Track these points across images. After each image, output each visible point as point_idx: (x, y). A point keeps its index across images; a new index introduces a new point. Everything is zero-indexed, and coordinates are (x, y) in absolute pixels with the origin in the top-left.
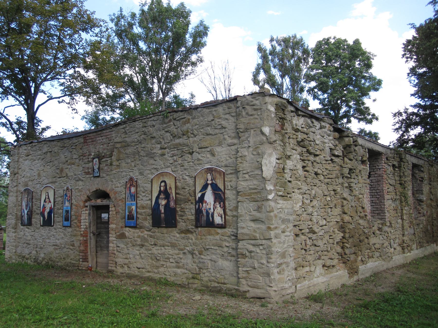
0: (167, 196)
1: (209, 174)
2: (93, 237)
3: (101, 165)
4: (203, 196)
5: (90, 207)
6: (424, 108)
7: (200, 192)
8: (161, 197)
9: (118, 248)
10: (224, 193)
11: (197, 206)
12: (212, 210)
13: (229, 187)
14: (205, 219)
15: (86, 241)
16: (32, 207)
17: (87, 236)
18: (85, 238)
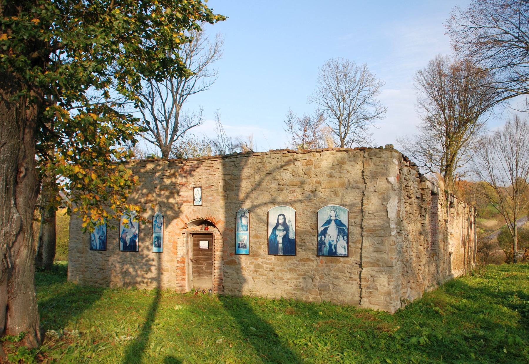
0: (286, 228)
1: (333, 212)
2: (191, 264)
3: (203, 195)
4: (326, 230)
5: (188, 235)
6: (118, 139)
7: (323, 226)
8: (278, 228)
9: (226, 274)
10: (348, 229)
11: (319, 239)
12: (335, 242)
13: (353, 224)
14: (328, 249)
15: (183, 268)
16: (107, 232)
17: (184, 263)
18: (182, 265)
